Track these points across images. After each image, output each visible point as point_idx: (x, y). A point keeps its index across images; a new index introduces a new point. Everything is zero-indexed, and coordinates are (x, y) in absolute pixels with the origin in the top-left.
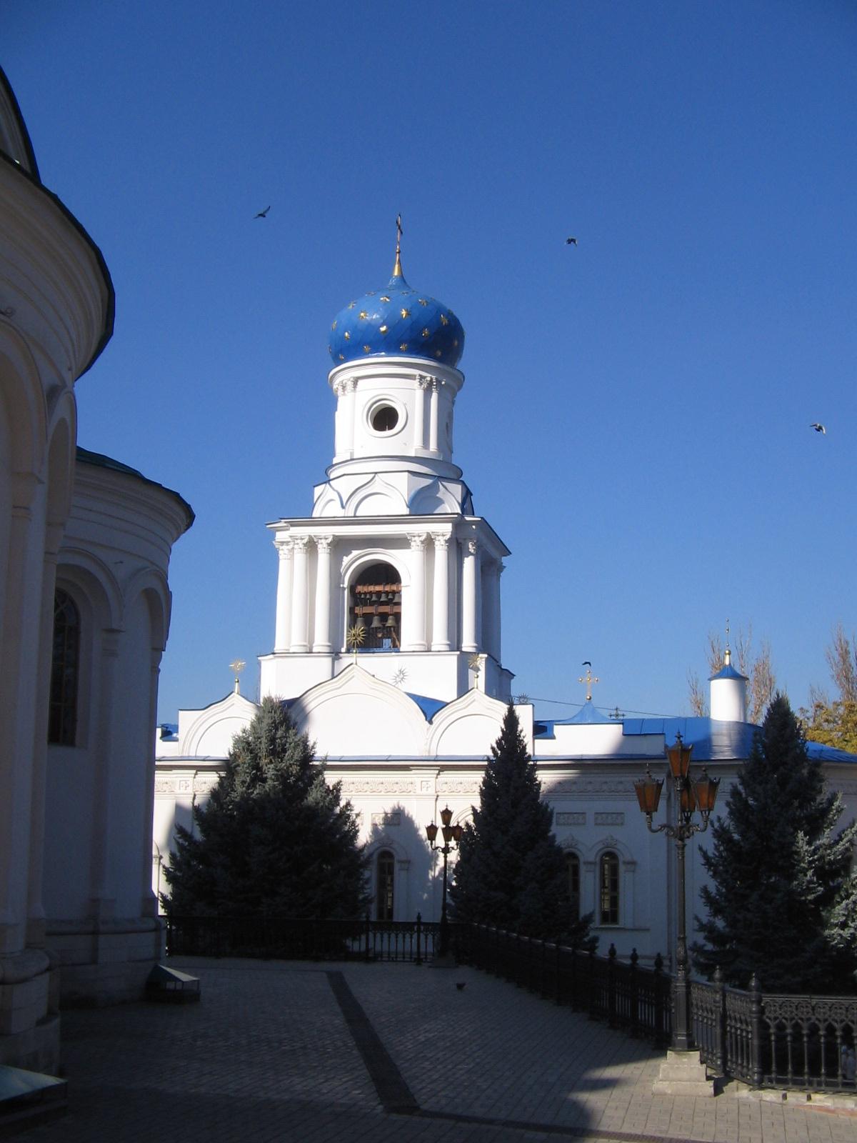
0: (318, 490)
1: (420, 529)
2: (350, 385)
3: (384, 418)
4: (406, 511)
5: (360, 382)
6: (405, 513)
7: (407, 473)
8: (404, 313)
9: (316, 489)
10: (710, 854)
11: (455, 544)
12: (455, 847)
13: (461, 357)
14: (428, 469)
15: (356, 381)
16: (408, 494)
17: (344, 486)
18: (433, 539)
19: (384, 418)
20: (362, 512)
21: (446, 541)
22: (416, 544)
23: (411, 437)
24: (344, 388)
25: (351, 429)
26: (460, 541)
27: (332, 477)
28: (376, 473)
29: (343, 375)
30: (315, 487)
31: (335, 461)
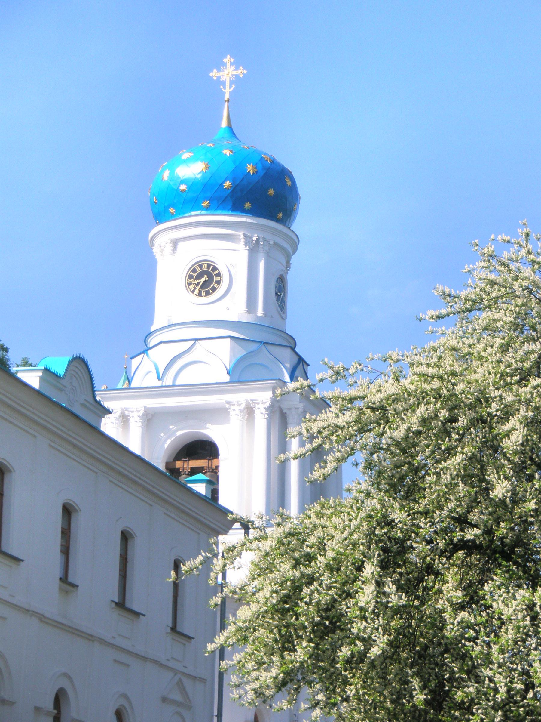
0: (135, 362)
1: (239, 398)
2: (169, 248)
3: (205, 278)
4: (226, 378)
5: (180, 245)
6: (226, 381)
7: (229, 340)
8: (227, 152)
9: (134, 361)
10: (228, 368)
11: (277, 415)
12: (272, 686)
13: (300, 198)
14: (231, 332)
15: (175, 243)
16: (230, 362)
17: (160, 355)
18: (252, 408)
19: (205, 278)
20: (184, 379)
21: (266, 409)
22: (236, 417)
23: (233, 303)
24: (162, 251)
25: (172, 299)
26: (284, 411)
27: (151, 345)
28: (196, 340)
29: (162, 236)
30: (132, 358)
31: (153, 329)
